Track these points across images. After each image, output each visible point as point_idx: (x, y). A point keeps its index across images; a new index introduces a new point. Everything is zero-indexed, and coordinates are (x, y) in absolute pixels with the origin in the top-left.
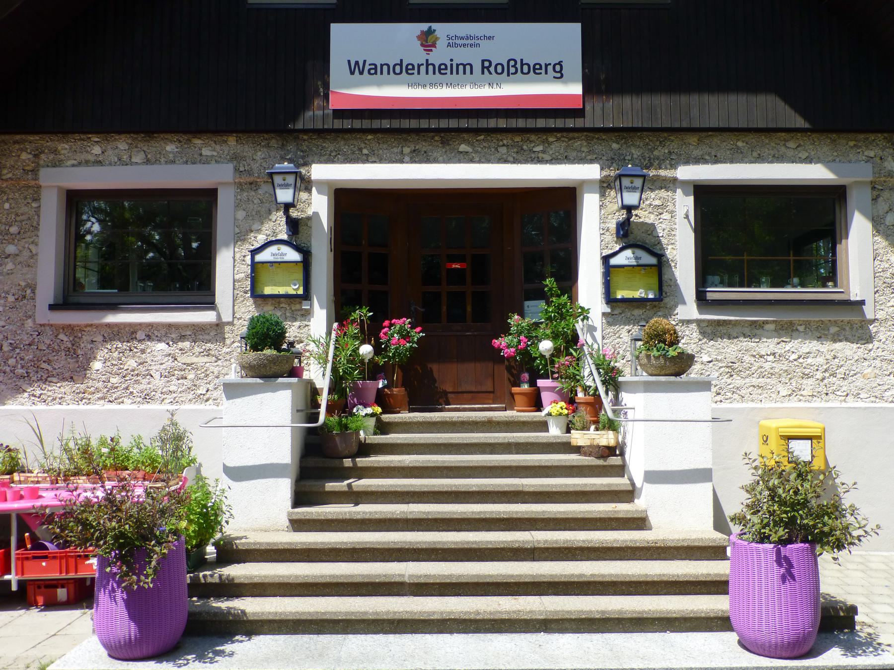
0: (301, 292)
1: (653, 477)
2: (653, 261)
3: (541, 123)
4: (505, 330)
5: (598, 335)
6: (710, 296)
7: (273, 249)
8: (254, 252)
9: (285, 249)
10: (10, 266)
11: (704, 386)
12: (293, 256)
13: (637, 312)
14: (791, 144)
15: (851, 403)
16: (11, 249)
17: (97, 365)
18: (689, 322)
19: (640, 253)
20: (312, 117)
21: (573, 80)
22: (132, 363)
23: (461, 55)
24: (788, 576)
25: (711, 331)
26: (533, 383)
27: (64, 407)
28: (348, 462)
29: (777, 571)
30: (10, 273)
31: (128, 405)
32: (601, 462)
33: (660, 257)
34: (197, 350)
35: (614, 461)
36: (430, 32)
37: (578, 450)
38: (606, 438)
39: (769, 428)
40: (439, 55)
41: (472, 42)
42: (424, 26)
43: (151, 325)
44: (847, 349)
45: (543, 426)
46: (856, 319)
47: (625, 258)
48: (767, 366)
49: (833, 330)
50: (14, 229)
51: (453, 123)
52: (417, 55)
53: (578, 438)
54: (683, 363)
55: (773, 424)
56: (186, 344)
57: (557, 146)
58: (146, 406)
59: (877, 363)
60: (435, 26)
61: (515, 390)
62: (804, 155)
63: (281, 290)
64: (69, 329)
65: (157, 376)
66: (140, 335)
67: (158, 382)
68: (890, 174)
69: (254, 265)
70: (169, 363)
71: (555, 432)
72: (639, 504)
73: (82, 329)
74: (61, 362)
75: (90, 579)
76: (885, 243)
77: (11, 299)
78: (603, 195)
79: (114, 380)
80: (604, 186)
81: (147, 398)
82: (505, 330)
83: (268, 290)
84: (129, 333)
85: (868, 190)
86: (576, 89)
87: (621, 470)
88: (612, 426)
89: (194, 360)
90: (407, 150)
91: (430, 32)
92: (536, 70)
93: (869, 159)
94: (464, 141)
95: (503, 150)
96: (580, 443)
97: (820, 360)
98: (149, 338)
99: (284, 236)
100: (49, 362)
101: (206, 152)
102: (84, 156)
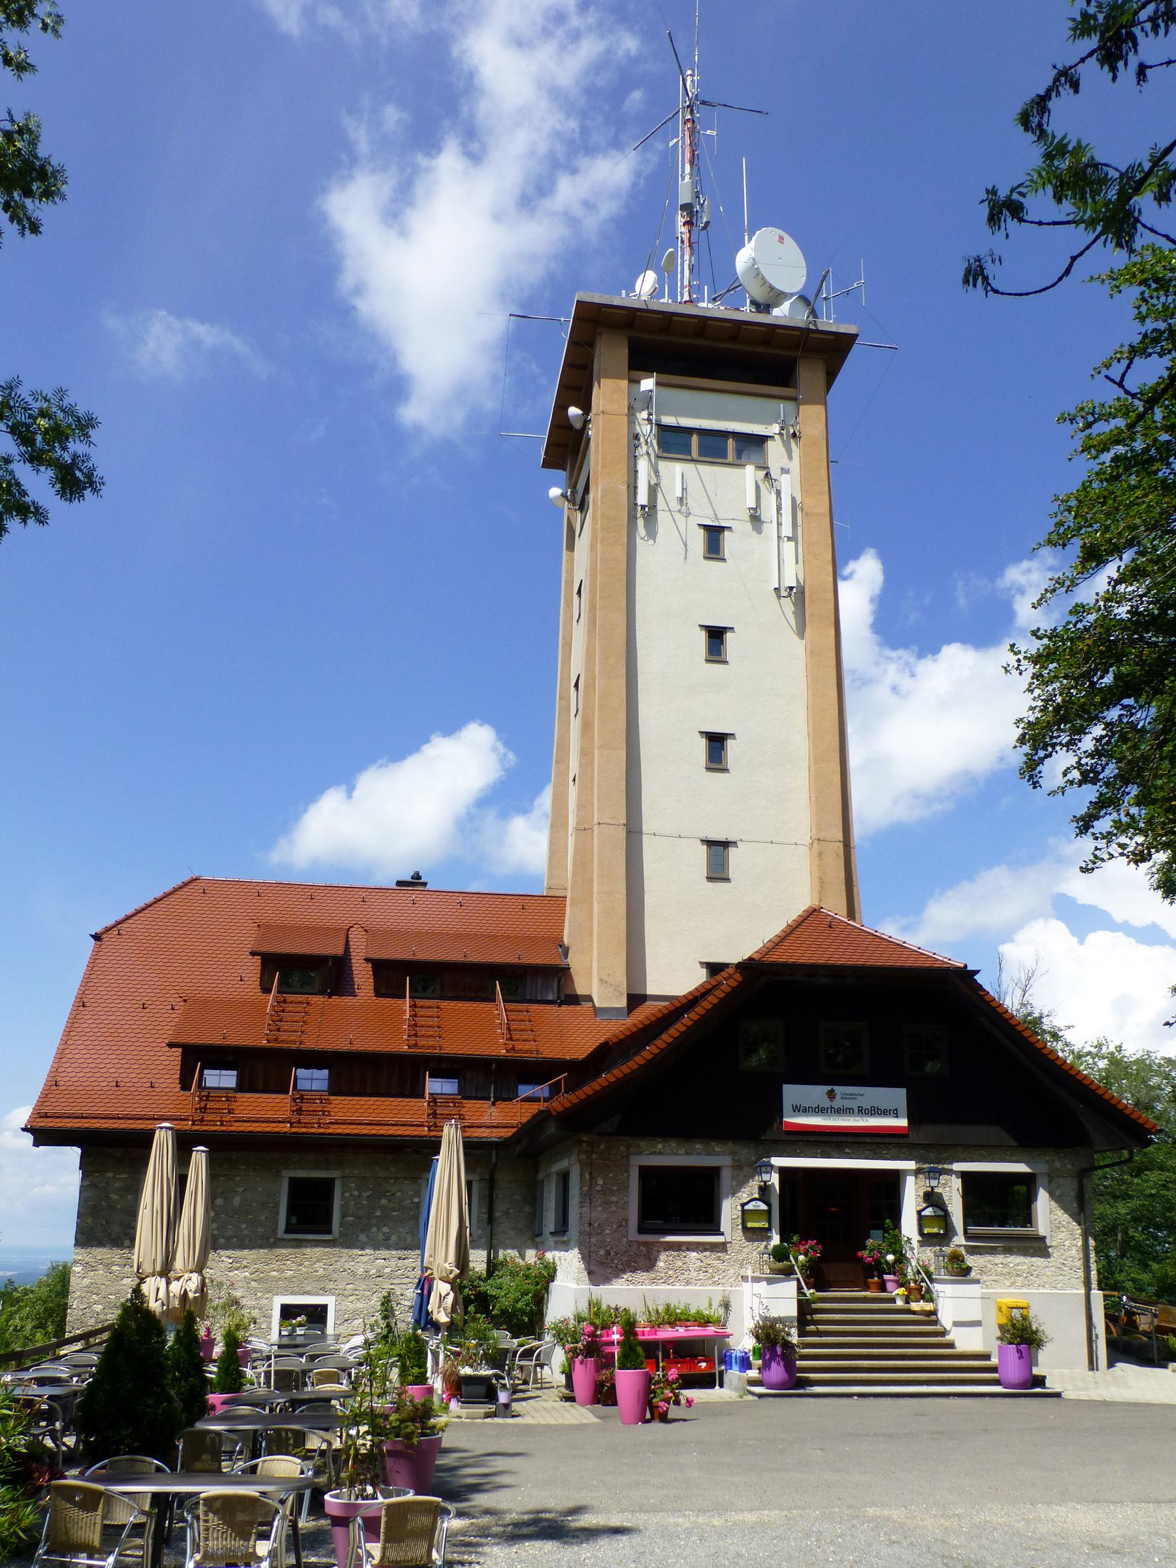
0: (767, 1226)
1: (957, 1324)
2: (941, 1213)
3: (887, 1140)
4: (864, 1248)
5: (915, 1252)
6: (969, 1231)
7: (753, 1203)
8: (743, 1205)
9: (759, 1203)
10: (614, 1208)
11: (977, 1282)
12: (764, 1207)
13: (934, 1240)
14: (1009, 1153)
15: (1042, 1291)
16: (614, 1199)
17: (661, 1264)
18: (960, 1246)
19: (936, 1209)
20: (770, 1135)
21: (903, 1117)
22: (679, 1263)
23: (848, 1104)
24: (1021, 1357)
25: (973, 1251)
26: (881, 1277)
27: (644, 1287)
28: (809, 1317)
29: (1017, 1355)
30: (614, 1212)
31: (677, 1287)
32: (927, 1318)
33: (946, 1211)
34: (713, 1257)
35: (933, 1318)
36: (832, 1091)
37: (914, 1313)
38: (929, 1307)
39: (1002, 1303)
40: (837, 1103)
41: (853, 1097)
42: (829, 1088)
43: (689, 1243)
44: (1038, 1261)
45: (893, 1300)
46: (1042, 1245)
47: (929, 1212)
48: (999, 1269)
49: (1031, 1251)
50: (615, 1188)
51: (843, 1139)
52: (826, 1103)
53: (914, 1306)
54: (968, 1270)
55: (1004, 1301)
56: (708, 1253)
57: (893, 1151)
58: (687, 1287)
59: (1053, 1269)
60: (835, 1087)
61: (870, 1280)
62: (1014, 1159)
63: (756, 1225)
64: (646, 1244)
65: (692, 1270)
66: (684, 1248)
67: (694, 1274)
68: (1172, 270)
69: (743, 1211)
70: (699, 1264)
71: (900, 1303)
72: (948, 1338)
73: (652, 1244)
74: (642, 1261)
75: (150, 1495)
76: (1056, 1205)
77: (615, 1226)
78: (916, 1177)
79: (670, 1272)
80: (917, 1172)
81: (688, 1283)
82: (864, 1248)
83: (749, 1225)
84: (677, 1247)
85: (1046, 1177)
86: (903, 1122)
87: (936, 1322)
88: (931, 1300)
89: (711, 1262)
90: (819, 1151)
91: (832, 1091)
92: (885, 1113)
93: (1047, 1162)
94: (848, 1147)
95: (867, 1152)
96: (916, 1309)
97: (1025, 1267)
98: (688, 1250)
99: (757, 1196)
100: (635, 1262)
101: (717, 1149)
102: (653, 1150)
